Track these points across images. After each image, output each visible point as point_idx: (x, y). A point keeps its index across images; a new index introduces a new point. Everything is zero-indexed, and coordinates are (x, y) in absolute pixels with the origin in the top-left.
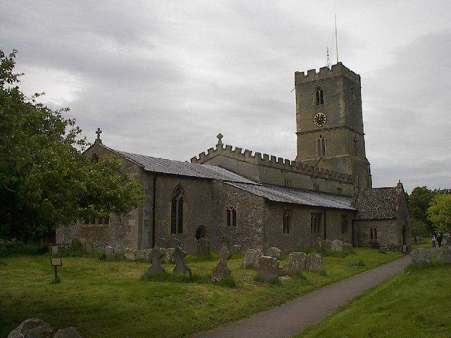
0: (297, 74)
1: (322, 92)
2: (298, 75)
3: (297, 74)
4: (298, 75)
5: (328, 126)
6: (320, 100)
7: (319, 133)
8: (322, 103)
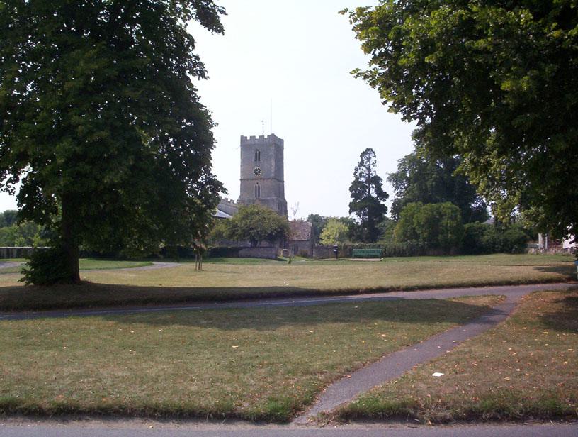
0: (242, 137)
2: (243, 139)
3: (242, 137)
4: (243, 139)
6: (257, 158)
7: (257, 181)
8: (259, 160)
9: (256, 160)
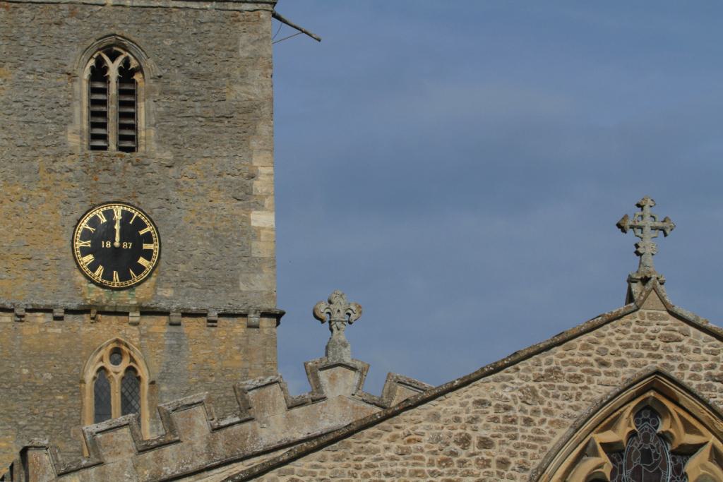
1: (127, 74)
5: (166, 295)
7: (107, 331)
8: (128, 141)
9: (97, 139)
